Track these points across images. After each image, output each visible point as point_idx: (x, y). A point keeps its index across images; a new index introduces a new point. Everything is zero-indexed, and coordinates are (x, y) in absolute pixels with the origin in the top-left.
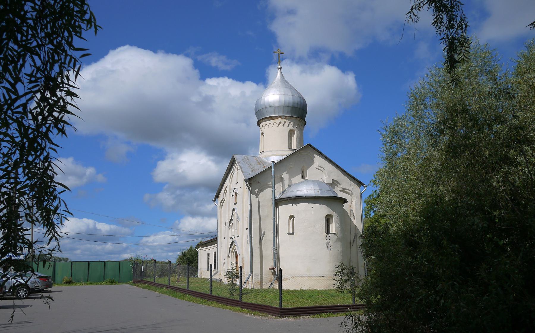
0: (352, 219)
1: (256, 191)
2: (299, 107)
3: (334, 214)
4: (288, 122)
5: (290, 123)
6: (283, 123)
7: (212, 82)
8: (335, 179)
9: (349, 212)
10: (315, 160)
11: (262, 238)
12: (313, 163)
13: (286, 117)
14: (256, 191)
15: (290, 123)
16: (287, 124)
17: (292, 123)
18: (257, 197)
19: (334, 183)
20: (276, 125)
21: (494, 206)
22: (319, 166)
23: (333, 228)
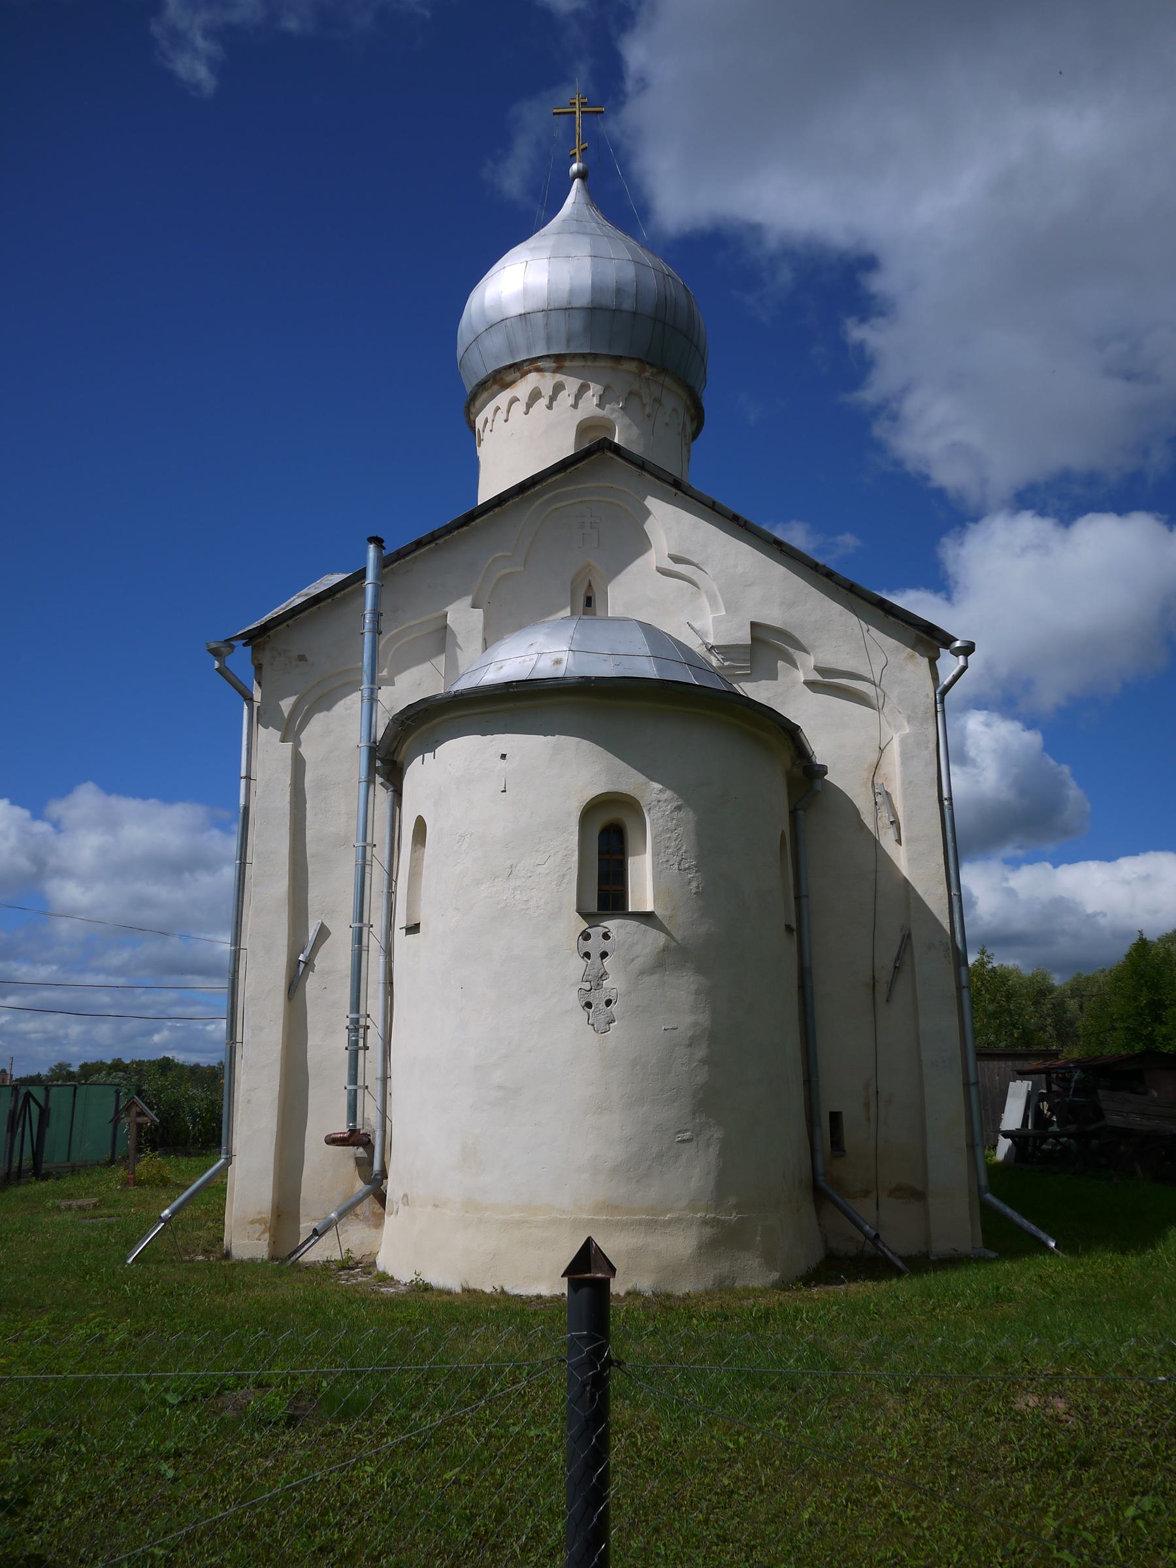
0: (887, 841)
1: (286, 705)
2: (628, 304)
3: (655, 798)
4: (572, 384)
5: (583, 389)
6: (547, 391)
7: (564, 446)
8: (773, 616)
9: (862, 801)
10: (650, 526)
11: (309, 964)
12: (642, 544)
13: (559, 362)
14: (286, 705)
15: (583, 389)
16: (566, 398)
17: (595, 389)
18: (291, 731)
19: (767, 645)
20: (519, 408)
21: (1065, 1032)
22: (676, 559)
23: (644, 883)
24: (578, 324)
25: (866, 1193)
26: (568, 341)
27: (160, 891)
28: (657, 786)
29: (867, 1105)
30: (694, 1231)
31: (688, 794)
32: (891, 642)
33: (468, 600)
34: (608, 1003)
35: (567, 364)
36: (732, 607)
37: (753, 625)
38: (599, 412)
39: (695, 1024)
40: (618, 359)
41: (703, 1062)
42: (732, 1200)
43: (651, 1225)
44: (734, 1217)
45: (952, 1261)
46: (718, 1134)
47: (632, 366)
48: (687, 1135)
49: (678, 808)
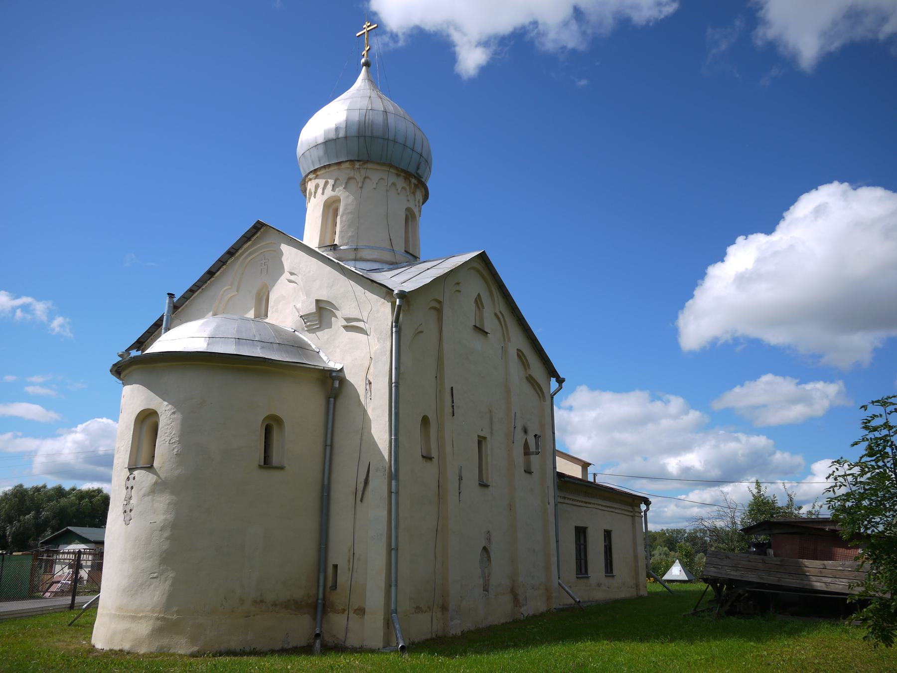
4: (321, 182)
6: (321, 186)
9: (361, 388)
24: (321, 152)
25: (344, 611)
26: (320, 161)
27: (627, 437)
28: (166, 403)
29: (349, 561)
30: (151, 622)
31: (178, 405)
32: (375, 297)
33: (211, 313)
34: (131, 510)
35: (318, 173)
36: (308, 294)
37: (317, 301)
38: (333, 194)
39: (165, 520)
40: (339, 163)
41: (167, 538)
42: (175, 609)
43: (134, 618)
44: (175, 617)
45: (373, 651)
46: (172, 575)
47: (347, 165)
48: (155, 575)
49: (174, 413)
